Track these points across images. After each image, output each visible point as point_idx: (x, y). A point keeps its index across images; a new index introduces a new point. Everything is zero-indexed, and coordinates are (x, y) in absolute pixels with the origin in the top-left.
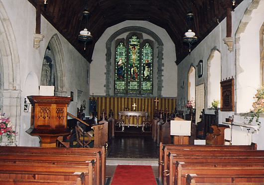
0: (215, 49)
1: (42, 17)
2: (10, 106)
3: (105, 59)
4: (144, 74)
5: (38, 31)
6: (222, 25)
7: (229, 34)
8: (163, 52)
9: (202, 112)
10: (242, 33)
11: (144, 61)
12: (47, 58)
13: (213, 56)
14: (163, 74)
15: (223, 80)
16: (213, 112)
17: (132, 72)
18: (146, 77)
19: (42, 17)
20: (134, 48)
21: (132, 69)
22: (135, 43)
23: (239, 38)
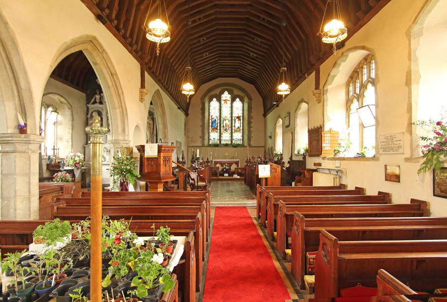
0: (302, 101)
1: (146, 73)
3: (200, 97)
5: (143, 86)
7: (317, 86)
10: (329, 86)
11: (235, 115)
12: (151, 115)
13: (300, 108)
16: (301, 158)
19: (147, 75)
23: (327, 90)
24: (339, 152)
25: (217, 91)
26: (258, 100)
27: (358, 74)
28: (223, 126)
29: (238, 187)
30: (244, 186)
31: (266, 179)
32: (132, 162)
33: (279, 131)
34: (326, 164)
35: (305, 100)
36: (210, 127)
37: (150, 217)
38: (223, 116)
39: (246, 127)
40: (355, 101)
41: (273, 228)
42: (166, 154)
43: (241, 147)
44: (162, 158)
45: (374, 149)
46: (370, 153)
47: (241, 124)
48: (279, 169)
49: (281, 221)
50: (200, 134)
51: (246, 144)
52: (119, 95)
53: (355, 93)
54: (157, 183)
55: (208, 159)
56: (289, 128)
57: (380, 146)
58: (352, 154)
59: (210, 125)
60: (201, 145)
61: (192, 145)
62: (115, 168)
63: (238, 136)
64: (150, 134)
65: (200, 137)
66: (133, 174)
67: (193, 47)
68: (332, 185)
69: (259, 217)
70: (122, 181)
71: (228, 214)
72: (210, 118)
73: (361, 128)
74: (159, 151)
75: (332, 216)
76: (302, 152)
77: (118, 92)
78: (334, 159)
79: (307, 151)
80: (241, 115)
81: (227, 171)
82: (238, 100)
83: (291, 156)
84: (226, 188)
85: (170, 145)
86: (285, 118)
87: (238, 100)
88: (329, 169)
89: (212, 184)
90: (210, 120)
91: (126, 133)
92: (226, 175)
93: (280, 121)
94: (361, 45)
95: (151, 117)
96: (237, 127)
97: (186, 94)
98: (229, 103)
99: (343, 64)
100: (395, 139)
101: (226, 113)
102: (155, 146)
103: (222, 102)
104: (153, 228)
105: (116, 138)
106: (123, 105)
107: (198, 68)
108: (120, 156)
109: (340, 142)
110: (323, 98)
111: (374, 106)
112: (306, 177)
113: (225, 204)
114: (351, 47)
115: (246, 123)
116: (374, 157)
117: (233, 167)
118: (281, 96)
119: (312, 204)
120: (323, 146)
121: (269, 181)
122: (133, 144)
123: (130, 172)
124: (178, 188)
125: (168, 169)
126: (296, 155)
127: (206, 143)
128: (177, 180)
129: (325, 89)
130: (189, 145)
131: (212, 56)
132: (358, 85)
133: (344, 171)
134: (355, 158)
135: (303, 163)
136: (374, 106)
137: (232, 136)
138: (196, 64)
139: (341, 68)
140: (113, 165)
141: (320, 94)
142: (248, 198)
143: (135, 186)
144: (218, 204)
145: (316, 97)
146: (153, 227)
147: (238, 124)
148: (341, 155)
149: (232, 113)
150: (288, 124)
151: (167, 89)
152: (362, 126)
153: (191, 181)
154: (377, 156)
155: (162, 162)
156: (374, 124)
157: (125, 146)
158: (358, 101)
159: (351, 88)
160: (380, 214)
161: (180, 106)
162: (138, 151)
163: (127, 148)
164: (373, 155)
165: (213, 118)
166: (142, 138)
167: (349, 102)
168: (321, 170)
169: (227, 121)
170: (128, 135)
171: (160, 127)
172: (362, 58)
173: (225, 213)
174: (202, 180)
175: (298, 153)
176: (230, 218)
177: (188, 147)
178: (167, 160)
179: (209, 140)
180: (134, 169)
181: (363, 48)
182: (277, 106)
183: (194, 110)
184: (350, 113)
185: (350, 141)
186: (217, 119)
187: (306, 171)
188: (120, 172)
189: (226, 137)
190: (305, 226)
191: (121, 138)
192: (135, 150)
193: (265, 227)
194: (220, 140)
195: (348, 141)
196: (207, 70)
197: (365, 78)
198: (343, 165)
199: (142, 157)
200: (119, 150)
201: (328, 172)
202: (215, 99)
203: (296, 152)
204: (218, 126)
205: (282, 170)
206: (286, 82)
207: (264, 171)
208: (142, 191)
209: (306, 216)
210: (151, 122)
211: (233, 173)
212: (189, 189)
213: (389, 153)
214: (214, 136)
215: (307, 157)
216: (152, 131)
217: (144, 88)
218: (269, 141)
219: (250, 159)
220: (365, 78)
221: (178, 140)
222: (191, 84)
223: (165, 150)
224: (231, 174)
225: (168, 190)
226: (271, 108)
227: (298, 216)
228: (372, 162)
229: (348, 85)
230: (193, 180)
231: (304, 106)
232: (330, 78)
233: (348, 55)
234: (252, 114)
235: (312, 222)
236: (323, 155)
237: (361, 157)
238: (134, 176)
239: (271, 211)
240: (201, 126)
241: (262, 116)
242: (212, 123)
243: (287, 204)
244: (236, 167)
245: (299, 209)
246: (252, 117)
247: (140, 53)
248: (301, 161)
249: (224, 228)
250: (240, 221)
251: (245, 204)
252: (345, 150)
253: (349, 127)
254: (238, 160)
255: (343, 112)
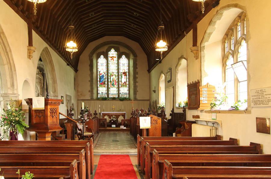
0: (182, 57)
1: (34, 32)
5: (30, 43)
6: (190, 35)
7: (195, 44)
8: (137, 63)
9: (171, 111)
11: (121, 71)
12: (41, 71)
13: (181, 64)
14: (137, 81)
15: (189, 83)
16: (181, 111)
18: (124, 83)
19: (34, 33)
23: (204, 47)
24: (215, 105)
25: (104, 49)
26: (143, 57)
27: (233, 32)
28: (111, 81)
29: (124, 137)
30: (129, 137)
31: (147, 130)
32: (20, 114)
33: (162, 85)
34: (204, 117)
35: (184, 56)
36: (99, 82)
37: (32, 164)
38: (110, 71)
39: (132, 82)
40: (230, 57)
41: (150, 174)
42: (53, 107)
43: (128, 100)
44: (49, 110)
45: (246, 103)
46: (243, 107)
47: (128, 79)
48: (160, 120)
49: (155, 169)
50: (89, 88)
51: (132, 97)
52: (7, 52)
53: (230, 49)
54: (45, 133)
55: (95, 111)
56: (171, 83)
57: (251, 100)
58: (226, 107)
59: (98, 79)
60: (90, 99)
61: (81, 98)
62: (5, 119)
63: (124, 90)
64: (41, 88)
65: (89, 91)
66: (21, 124)
67: (78, 7)
68: (209, 136)
69: (139, 165)
70: (11, 131)
71: (111, 162)
72: (98, 74)
73: (236, 82)
74: (46, 104)
75: (203, 164)
76: (183, 105)
77: (6, 49)
78: (211, 112)
79: (187, 104)
80: (127, 71)
81: (115, 123)
82: (124, 56)
83: (173, 109)
84: (112, 138)
85: (60, 98)
86: (167, 73)
87: (124, 56)
88: (206, 121)
89: (100, 134)
90: (98, 76)
91: (15, 87)
92: (114, 126)
93: (163, 77)
94: (234, 3)
95: (41, 73)
96: (123, 82)
97: (69, 51)
98: (116, 59)
99: (218, 22)
100: (265, 93)
101: (113, 68)
102: (42, 99)
103: (110, 59)
104: (18, 174)
105: (6, 92)
106: (11, 61)
107: (86, 27)
108: (9, 108)
109: (216, 95)
110: (201, 55)
111: (246, 62)
112: (186, 129)
113: (109, 152)
114: (224, 5)
115: (132, 78)
116: (246, 110)
117: (120, 119)
118: (159, 52)
119: (186, 153)
120: (201, 99)
121: (150, 131)
122: (22, 97)
123: (18, 122)
124: (66, 138)
125: (55, 120)
126: (177, 108)
127: (95, 96)
128: (66, 131)
129: (202, 46)
130: (79, 99)
131: (98, 16)
132: (233, 42)
133: (220, 123)
134: (230, 111)
135: (183, 115)
136: (246, 62)
137: (119, 91)
138: (83, 24)
139: (216, 26)
140: (3, 117)
141: (198, 50)
142: (131, 147)
143: (25, 135)
144: (103, 152)
145: (194, 53)
146: (18, 172)
147: (124, 79)
148: (216, 108)
149: (118, 69)
150: (169, 79)
151: (55, 47)
152: (237, 81)
153: (78, 132)
154: (249, 109)
155: (49, 114)
156: (246, 79)
157: (14, 99)
158: (233, 57)
159: (226, 45)
160: (249, 163)
161: (69, 62)
162: (27, 104)
163: (16, 101)
164: (246, 108)
165: (101, 74)
166: (32, 94)
167: (224, 58)
168: (199, 122)
169: (114, 76)
170: (17, 89)
171: (50, 81)
172: (236, 16)
173: (108, 161)
174: (89, 130)
175: (179, 106)
176: (112, 165)
177: (78, 100)
178: (54, 112)
179: (97, 93)
180: (23, 120)
181: (236, 6)
182: (160, 62)
183: (83, 66)
184: (226, 68)
185: (226, 95)
186: (104, 75)
187: (185, 123)
188: (9, 123)
189: (113, 91)
190: (173, 174)
191: (10, 92)
192: (24, 103)
193: (144, 174)
194: (108, 94)
195: (224, 94)
196: (94, 29)
197: (239, 35)
198: (219, 118)
199: (30, 109)
200: (9, 103)
201: (205, 124)
202: (102, 56)
203: (177, 106)
204: (106, 81)
205: (163, 122)
206: (164, 40)
207: (145, 123)
208: (32, 140)
209: (174, 164)
210: (42, 78)
211: (120, 124)
212: (77, 139)
213: (260, 106)
214: (102, 90)
215: (187, 110)
216: (42, 85)
217: (32, 46)
218: (154, 95)
219: (135, 112)
220: (239, 35)
221: (68, 94)
222: (74, 41)
223: (51, 103)
224: (118, 125)
225: (56, 139)
226: (155, 64)
227: (167, 164)
228: (244, 115)
229: (224, 42)
230: (80, 130)
231: (184, 62)
232: (207, 35)
233: (222, 13)
234: (137, 70)
235: (180, 170)
236: (201, 108)
237: (235, 110)
238: (23, 126)
239: (148, 160)
240: (89, 81)
241: (147, 72)
242: (100, 79)
243: (159, 153)
244: (123, 119)
245: (168, 158)
246: (137, 73)
247: (27, 13)
248: (182, 113)
249: (105, 175)
250: (122, 168)
251: (128, 152)
252: (221, 104)
253: (225, 81)
254: (125, 112)
255: (219, 67)
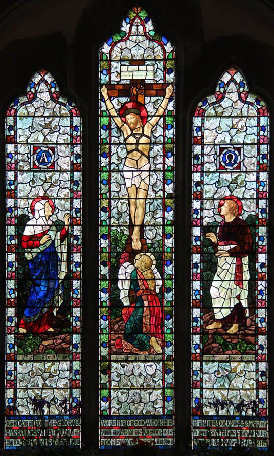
2: (142, 180)
4: (206, 304)
17: (124, 287)
18: (227, 322)
20: (139, 107)
21: (126, 270)
22: (143, 74)
